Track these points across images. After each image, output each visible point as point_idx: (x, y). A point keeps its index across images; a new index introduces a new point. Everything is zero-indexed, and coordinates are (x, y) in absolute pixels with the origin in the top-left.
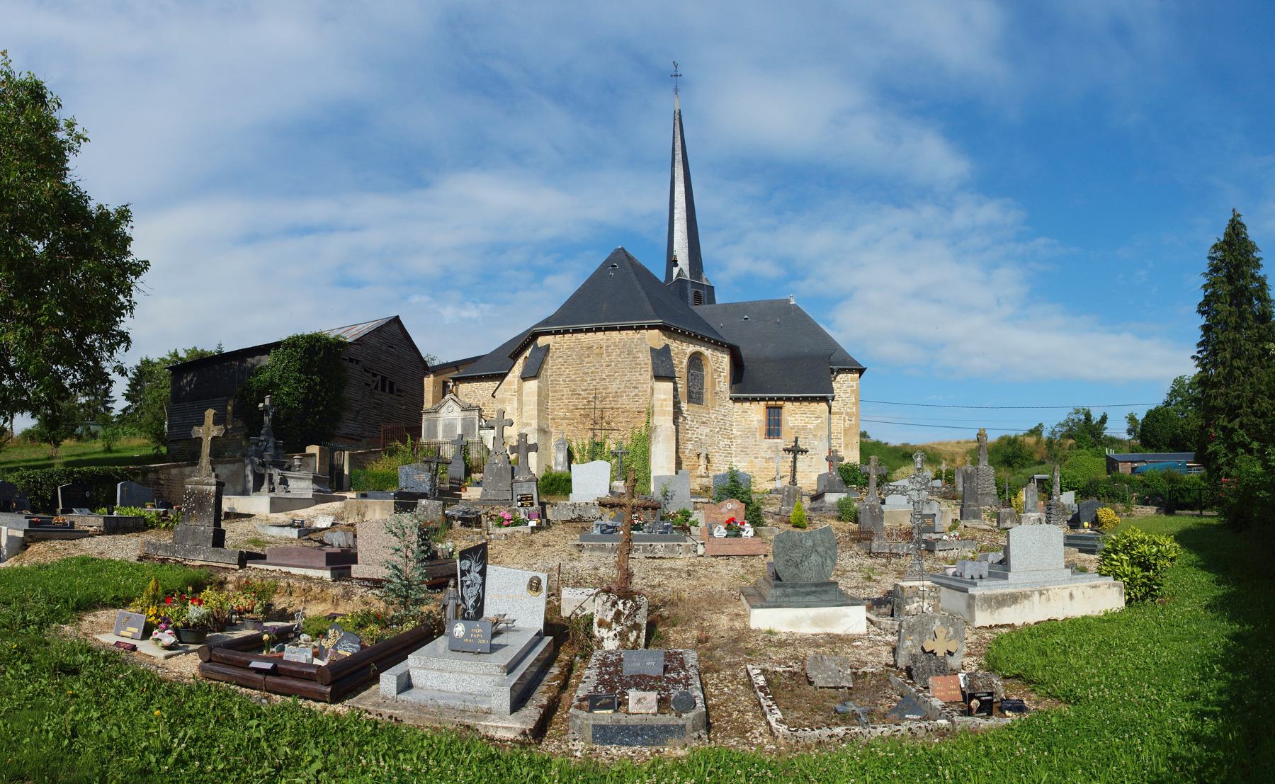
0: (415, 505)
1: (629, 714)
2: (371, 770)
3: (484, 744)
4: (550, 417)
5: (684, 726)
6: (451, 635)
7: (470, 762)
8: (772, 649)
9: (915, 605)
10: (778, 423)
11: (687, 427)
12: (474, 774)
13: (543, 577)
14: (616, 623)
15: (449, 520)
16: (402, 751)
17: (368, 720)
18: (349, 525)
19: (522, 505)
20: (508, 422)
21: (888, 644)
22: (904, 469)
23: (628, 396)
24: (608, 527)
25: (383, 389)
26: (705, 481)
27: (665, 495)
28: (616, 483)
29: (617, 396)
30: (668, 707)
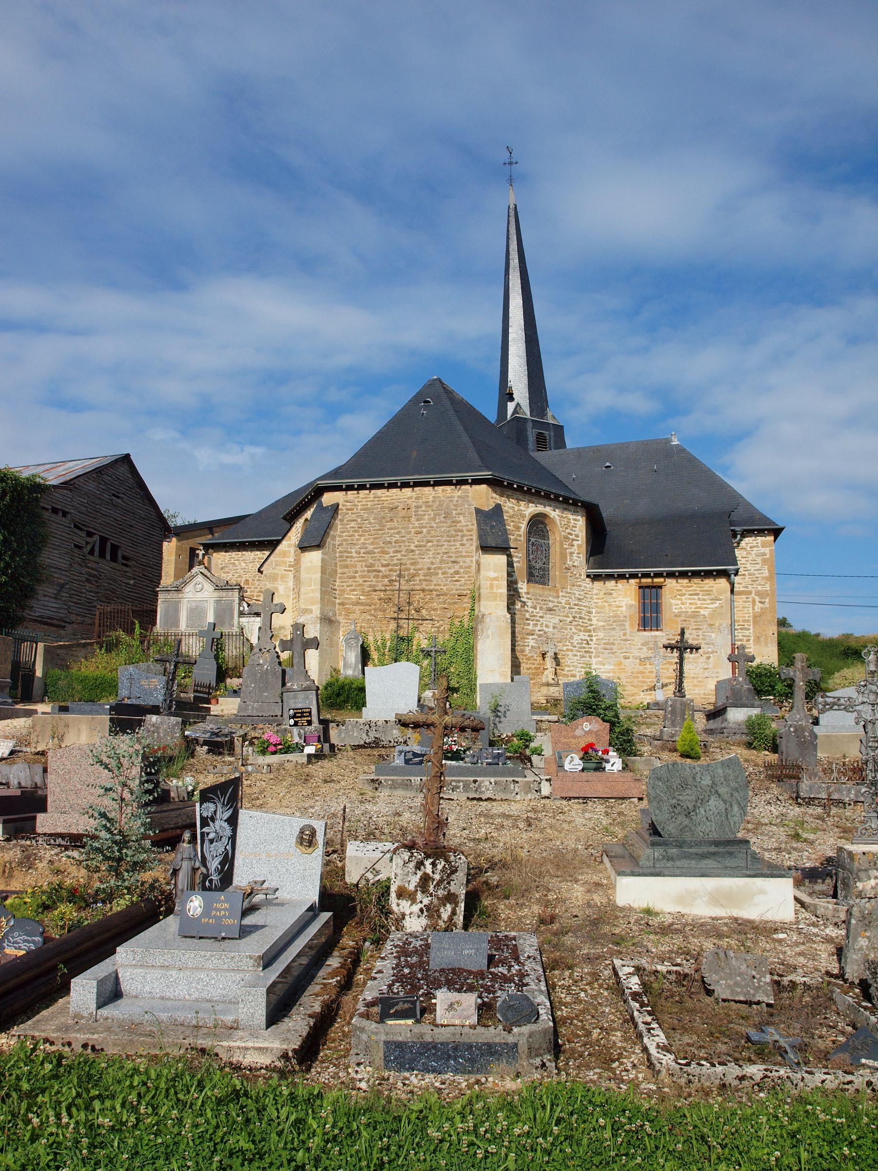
0: (140, 723)
1: (437, 1026)
2: (46, 1133)
4: (337, 601)
5: (516, 1045)
6: (183, 913)
7: (203, 1105)
8: (652, 937)
9: (873, 882)
12: (207, 1122)
13: (319, 826)
14: (423, 892)
15: (190, 745)
16: (99, 1097)
18: (38, 753)
19: (296, 724)
20: (278, 608)
21: (829, 940)
22: (846, 672)
23: (443, 573)
24: (415, 755)
25: (102, 555)
27: (495, 710)
28: (428, 694)
29: (430, 573)
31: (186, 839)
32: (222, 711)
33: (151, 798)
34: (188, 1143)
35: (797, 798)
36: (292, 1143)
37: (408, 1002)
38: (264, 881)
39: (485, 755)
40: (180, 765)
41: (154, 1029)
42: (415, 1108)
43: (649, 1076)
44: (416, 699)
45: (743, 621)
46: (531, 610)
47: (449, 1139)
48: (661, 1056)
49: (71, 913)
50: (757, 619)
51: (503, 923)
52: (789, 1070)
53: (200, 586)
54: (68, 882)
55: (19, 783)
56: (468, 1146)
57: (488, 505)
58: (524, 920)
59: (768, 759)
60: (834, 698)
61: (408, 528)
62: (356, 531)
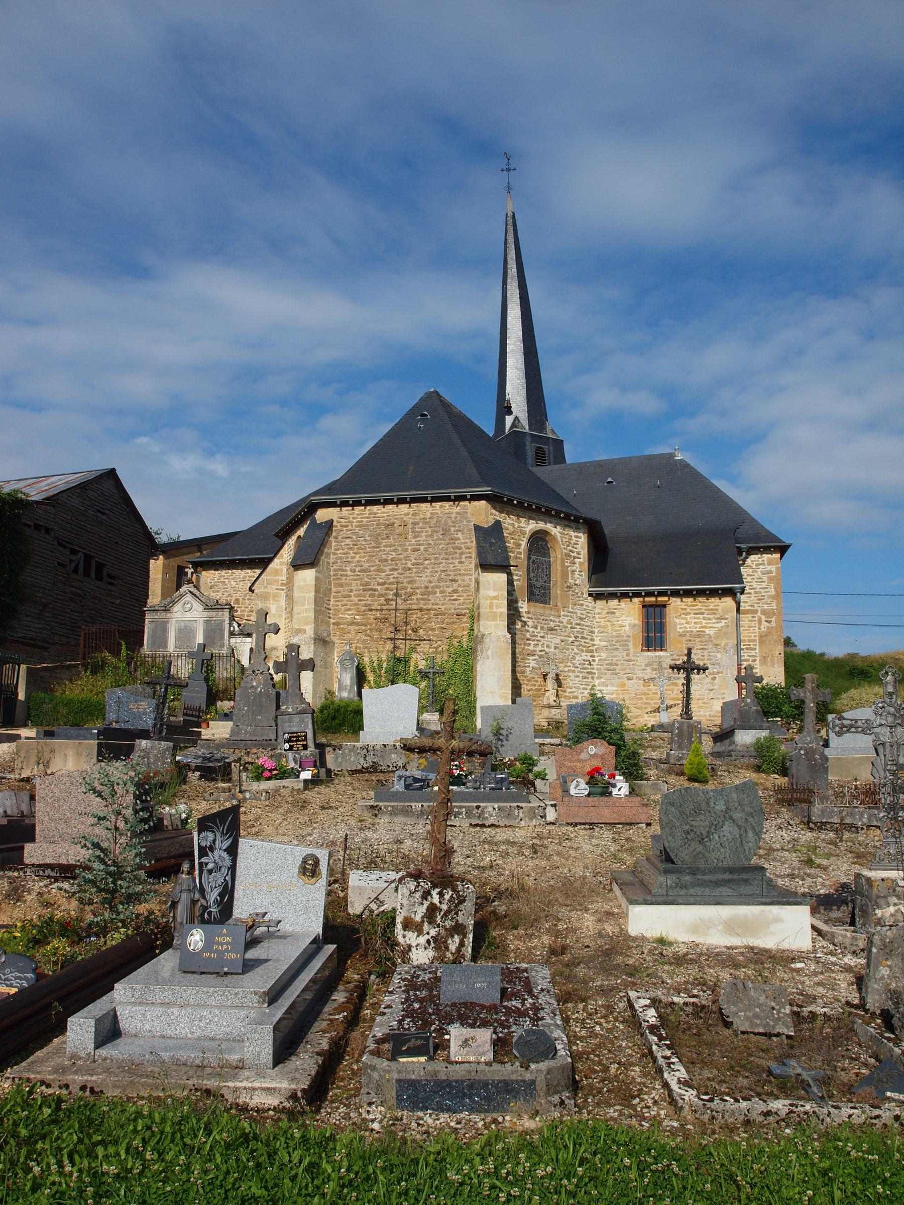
0: (130, 750)
1: (451, 1063)
3: (232, 1118)
4: (332, 621)
5: (533, 1082)
6: (183, 947)
8: (666, 967)
9: (892, 909)
10: (661, 628)
11: (528, 635)
13: (322, 855)
14: (430, 923)
16: (102, 1142)
17: (45, 1097)
18: (22, 780)
19: (291, 748)
20: (272, 628)
21: (848, 969)
22: (853, 692)
23: (441, 592)
24: (416, 780)
25: (87, 573)
26: (555, 714)
27: (497, 733)
28: (426, 716)
29: (428, 592)
30: (509, 1053)
31: (185, 870)
32: (213, 735)
33: (146, 827)
34: (198, 1191)
35: (808, 822)
36: (307, 1189)
37: (421, 1038)
38: (266, 913)
39: (488, 780)
40: (172, 791)
41: (157, 1069)
42: (432, 1150)
43: (671, 1112)
44: (416, 722)
45: (749, 641)
46: (531, 630)
47: (469, 1182)
48: (683, 1092)
49: (64, 948)
50: (763, 638)
51: (512, 955)
52: (814, 1105)
53: (189, 606)
54: (59, 915)
55: (5, 812)
56: (490, 1190)
57: (487, 522)
58: (534, 951)
59: (778, 782)
60: (851, 720)
61: (405, 545)
62: (350, 549)
